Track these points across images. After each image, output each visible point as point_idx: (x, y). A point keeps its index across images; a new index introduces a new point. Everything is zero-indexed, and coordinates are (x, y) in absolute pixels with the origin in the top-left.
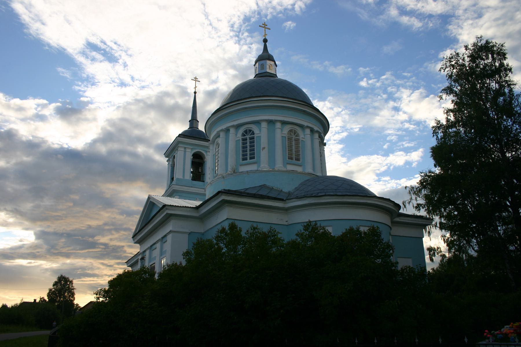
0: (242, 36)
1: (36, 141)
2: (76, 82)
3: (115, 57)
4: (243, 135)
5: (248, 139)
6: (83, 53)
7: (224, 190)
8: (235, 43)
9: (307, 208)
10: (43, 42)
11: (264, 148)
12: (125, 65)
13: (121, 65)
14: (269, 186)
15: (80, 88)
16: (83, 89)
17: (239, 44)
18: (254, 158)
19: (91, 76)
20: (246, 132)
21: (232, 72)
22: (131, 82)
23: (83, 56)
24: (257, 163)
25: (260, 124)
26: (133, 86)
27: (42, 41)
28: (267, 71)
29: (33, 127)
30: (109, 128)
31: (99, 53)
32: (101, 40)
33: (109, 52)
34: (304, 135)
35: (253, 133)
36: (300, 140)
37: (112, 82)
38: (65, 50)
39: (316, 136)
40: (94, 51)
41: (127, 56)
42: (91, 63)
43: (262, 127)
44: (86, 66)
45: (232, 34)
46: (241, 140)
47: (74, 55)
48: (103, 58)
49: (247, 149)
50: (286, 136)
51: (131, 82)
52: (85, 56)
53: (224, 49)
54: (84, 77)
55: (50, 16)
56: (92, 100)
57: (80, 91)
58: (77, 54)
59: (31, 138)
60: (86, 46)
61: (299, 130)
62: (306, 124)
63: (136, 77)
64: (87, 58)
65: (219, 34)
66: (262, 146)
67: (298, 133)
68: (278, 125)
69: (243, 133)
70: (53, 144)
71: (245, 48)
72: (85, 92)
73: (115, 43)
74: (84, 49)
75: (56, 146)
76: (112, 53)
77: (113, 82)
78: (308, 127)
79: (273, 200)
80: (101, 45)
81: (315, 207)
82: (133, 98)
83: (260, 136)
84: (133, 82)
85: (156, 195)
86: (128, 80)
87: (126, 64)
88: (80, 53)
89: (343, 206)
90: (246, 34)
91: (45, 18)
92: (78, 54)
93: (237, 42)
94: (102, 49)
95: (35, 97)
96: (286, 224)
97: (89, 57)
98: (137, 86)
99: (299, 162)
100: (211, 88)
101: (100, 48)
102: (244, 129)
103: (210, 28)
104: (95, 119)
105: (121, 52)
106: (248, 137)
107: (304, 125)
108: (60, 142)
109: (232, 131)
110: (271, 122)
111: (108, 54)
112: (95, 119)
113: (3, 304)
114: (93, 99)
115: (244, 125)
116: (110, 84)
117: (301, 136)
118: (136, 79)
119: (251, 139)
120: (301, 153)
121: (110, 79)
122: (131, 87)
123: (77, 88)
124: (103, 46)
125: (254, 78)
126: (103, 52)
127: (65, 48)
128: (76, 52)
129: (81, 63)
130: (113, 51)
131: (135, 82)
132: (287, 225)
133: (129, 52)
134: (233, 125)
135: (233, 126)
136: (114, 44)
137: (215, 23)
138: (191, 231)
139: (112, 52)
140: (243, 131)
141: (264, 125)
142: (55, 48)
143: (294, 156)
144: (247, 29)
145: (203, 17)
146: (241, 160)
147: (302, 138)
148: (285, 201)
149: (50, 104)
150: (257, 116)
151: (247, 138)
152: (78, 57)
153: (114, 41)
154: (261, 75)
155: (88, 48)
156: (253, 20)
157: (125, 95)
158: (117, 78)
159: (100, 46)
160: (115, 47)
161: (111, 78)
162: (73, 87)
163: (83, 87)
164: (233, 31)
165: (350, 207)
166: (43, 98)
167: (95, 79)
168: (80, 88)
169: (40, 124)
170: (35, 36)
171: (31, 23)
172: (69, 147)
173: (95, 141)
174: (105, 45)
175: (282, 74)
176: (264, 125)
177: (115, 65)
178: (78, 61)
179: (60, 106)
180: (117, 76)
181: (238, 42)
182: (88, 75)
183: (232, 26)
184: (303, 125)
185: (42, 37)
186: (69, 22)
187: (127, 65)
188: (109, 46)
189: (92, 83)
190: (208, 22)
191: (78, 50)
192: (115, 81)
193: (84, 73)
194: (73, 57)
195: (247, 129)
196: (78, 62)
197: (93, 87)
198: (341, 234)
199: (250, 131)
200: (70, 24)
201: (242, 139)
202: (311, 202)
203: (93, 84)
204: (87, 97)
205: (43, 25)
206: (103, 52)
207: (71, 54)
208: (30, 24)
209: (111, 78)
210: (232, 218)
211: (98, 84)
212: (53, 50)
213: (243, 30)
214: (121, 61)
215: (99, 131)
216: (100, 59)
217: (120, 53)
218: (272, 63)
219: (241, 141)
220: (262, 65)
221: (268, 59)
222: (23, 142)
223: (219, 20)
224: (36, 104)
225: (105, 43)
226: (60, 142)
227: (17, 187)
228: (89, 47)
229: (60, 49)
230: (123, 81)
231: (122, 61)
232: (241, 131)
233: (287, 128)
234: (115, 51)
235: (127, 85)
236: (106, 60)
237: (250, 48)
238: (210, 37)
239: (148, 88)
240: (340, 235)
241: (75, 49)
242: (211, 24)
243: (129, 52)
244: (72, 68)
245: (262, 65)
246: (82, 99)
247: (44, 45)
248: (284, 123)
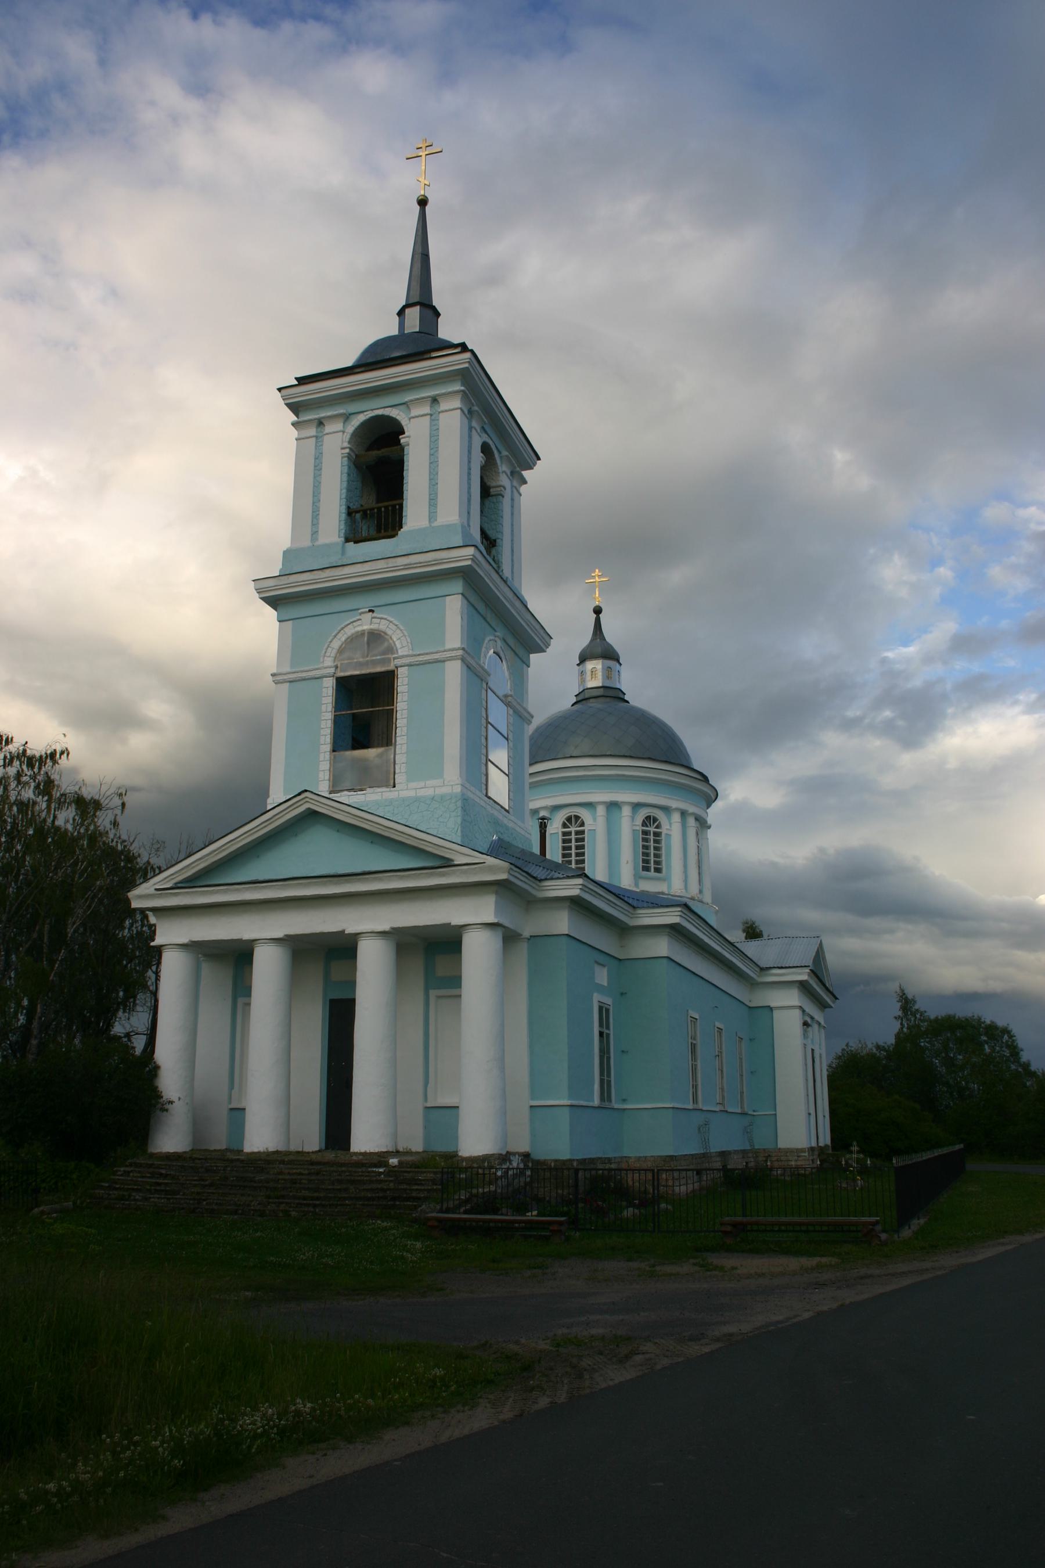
5: (573, 833)
24: (667, 879)
25: (596, 808)
35: (582, 824)
36: (663, 835)
39: (691, 822)
43: (598, 814)
46: (560, 834)
50: (640, 828)
62: (674, 804)
67: (660, 822)
68: (626, 811)
69: (564, 822)
78: (677, 809)
85: (802, 936)
106: (573, 829)
110: (613, 806)
113: (1022, 1050)
119: (577, 833)
120: (663, 858)
143: (652, 865)
146: (641, 869)
147: (667, 829)
199: (577, 818)
219: (560, 837)
240: (957, 1017)
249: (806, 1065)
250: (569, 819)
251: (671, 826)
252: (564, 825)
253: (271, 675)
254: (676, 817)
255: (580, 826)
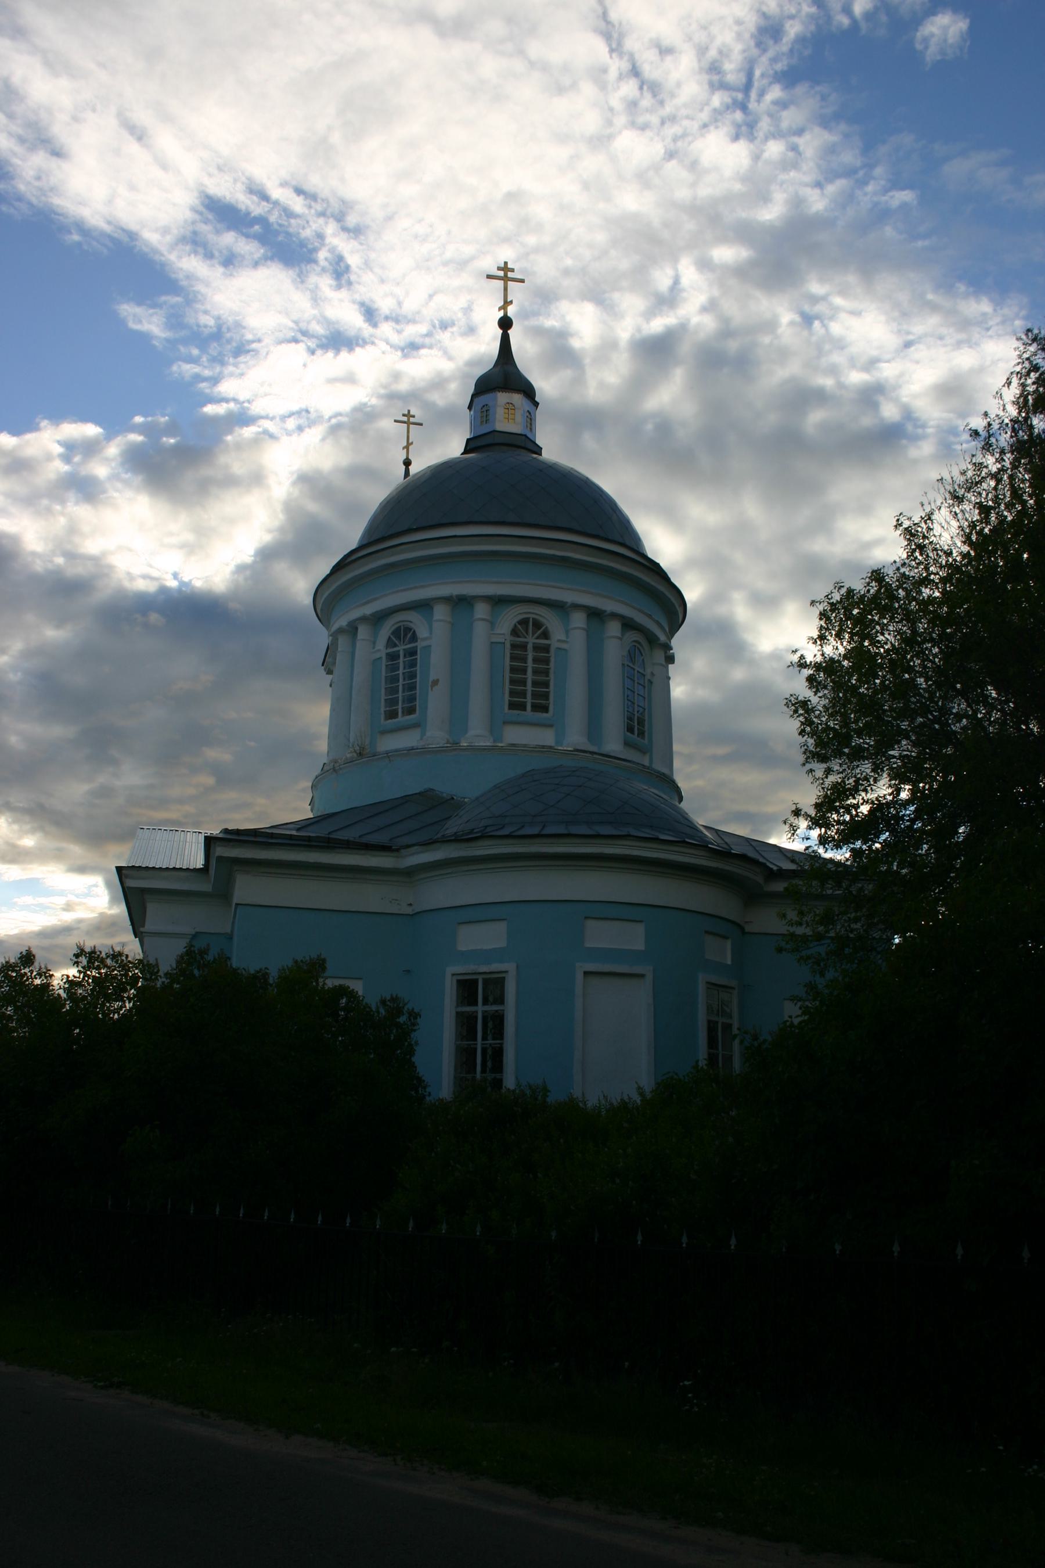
0: (761, 105)
1: (78, 570)
2: (182, 349)
3: (302, 244)
4: (390, 643)
5: (402, 654)
6: (194, 242)
7: (226, 831)
8: (736, 138)
9: (450, 871)
10: (61, 218)
11: (435, 682)
12: (340, 271)
13: (324, 270)
14: (442, 793)
15: (197, 369)
16: (207, 373)
17: (751, 138)
18: (545, 709)
19: (231, 320)
20: (396, 633)
21: (726, 254)
22: (367, 330)
23: (196, 253)
25: (432, 608)
26: (373, 343)
27: (59, 215)
28: (498, 429)
29: (62, 520)
30: (313, 507)
31: (247, 236)
32: (246, 181)
33: (280, 225)
34: (567, 632)
35: (414, 638)
36: (552, 650)
37: (299, 336)
38: (132, 236)
40: (229, 228)
41: (344, 235)
42: (224, 274)
44: (207, 284)
45: (717, 100)
46: (508, 645)
47: (164, 249)
48: (262, 251)
49: (398, 686)
50: (509, 639)
51: (367, 330)
52: (201, 250)
53: (694, 166)
54: (206, 326)
55: (76, 119)
56: (243, 408)
57: (198, 378)
58: (173, 247)
59: (60, 560)
60: (201, 214)
61: (550, 620)
62: (569, 597)
63: (385, 305)
64: (209, 256)
65: (668, 109)
66: (433, 676)
67: (546, 627)
68: (481, 610)
70: (131, 577)
71: (775, 149)
72: (215, 380)
73: (299, 191)
74: (194, 223)
75: (142, 585)
76: (291, 230)
77: (305, 333)
79: (363, 852)
80: (249, 202)
81: (466, 868)
82: (382, 391)
83: (430, 646)
84: (375, 325)
86: (353, 320)
87: (342, 265)
88: (183, 240)
89: (475, 868)
90: (775, 93)
91: (59, 129)
92: (176, 244)
93: (744, 128)
94: (255, 218)
95: (57, 416)
96: (409, 911)
97: (217, 254)
98: (388, 343)
99: (545, 715)
100: (658, 325)
101: (248, 214)
102: (393, 625)
103: (629, 88)
104: (257, 479)
105: (321, 221)
107: (565, 601)
108: (151, 566)
109: (363, 632)
110: (461, 603)
111: (277, 233)
112: (257, 479)
114: (246, 405)
115: (394, 615)
116: (293, 345)
117: (557, 634)
118: (383, 316)
121: (292, 325)
122: (369, 348)
123: (189, 369)
124: (258, 209)
125: (406, 480)
126: (260, 230)
127: (133, 227)
128: (169, 238)
129: (189, 277)
130: (293, 221)
131: (380, 325)
132: (412, 915)
133: (351, 220)
134: (362, 615)
135: (363, 619)
136: (294, 195)
137: (651, 66)
138: (198, 930)
139: (290, 225)
140: (390, 632)
141: (440, 612)
142: (103, 234)
144: (776, 73)
145: (601, 48)
146: (383, 716)
147: (559, 641)
148: (398, 850)
149: (109, 437)
150: (422, 587)
151: (399, 651)
152: (180, 257)
153: (294, 183)
154: (479, 443)
155: (206, 222)
156: (793, 30)
157: (350, 379)
158: (314, 317)
159: (247, 207)
160: (297, 205)
161: (296, 322)
162: (175, 368)
163: (206, 364)
164: (723, 86)
165: (530, 866)
166: (84, 418)
167: (244, 328)
168: (197, 369)
169: (82, 512)
170: (34, 201)
171: (15, 154)
172: (187, 584)
173: (267, 555)
174: (264, 204)
175: (927, 243)
176: (440, 612)
177: (305, 272)
178: (181, 269)
179: (143, 443)
180: (315, 312)
181: (745, 130)
182: (218, 318)
183: (714, 68)
184: (562, 602)
185: (56, 201)
186: (139, 134)
187: (348, 268)
188: (276, 203)
189: (234, 344)
190: (625, 65)
191: (175, 231)
192: (311, 332)
193: (206, 312)
194: (163, 259)
195: (399, 625)
196: (181, 276)
197: (242, 359)
198: (151, 962)
200: (140, 139)
201: (387, 654)
202: (452, 856)
203: (241, 350)
204: (226, 400)
205: (54, 159)
206: (260, 230)
207: (155, 251)
208: (16, 161)
209: (296, 322)
210: (250, 903)
211: (254, 346)
212: (95, 243)
213: (763, 75)
214: (322, 255)
215: (280, 518)
216: (252, 253)
217: (317, 224)
218: (517, 398)
220: (485, 409)
221: (502, 388)
222: (36, 579)
223: (665, 51)
224: (59, 442)
225: (264, 197)
226: (151, 566)
227: (37, 730)
228: (210, 216)
229: (116, 235)
230: (336, 326)
231: (328, 255)
232: (386, 630)
233: (510, 617)
234: (299, 221)
235: (354, 342)
236: (272, 259)
237: (794, 148)
238: (633, 124)
239: (431, 347)
241: (165, 231)
242: (635, 72)
243: (351, 220)
244: (163, 298)
245: (485, 409)
246: (210, 409)
247: (64, 229)
248: (499, 602)
249: (585, 870)
250: (524, 622)
251: (567, 637)
252: (515, 632)
253: (986, 412)
254: (579, 619)
255: (410, 643)
